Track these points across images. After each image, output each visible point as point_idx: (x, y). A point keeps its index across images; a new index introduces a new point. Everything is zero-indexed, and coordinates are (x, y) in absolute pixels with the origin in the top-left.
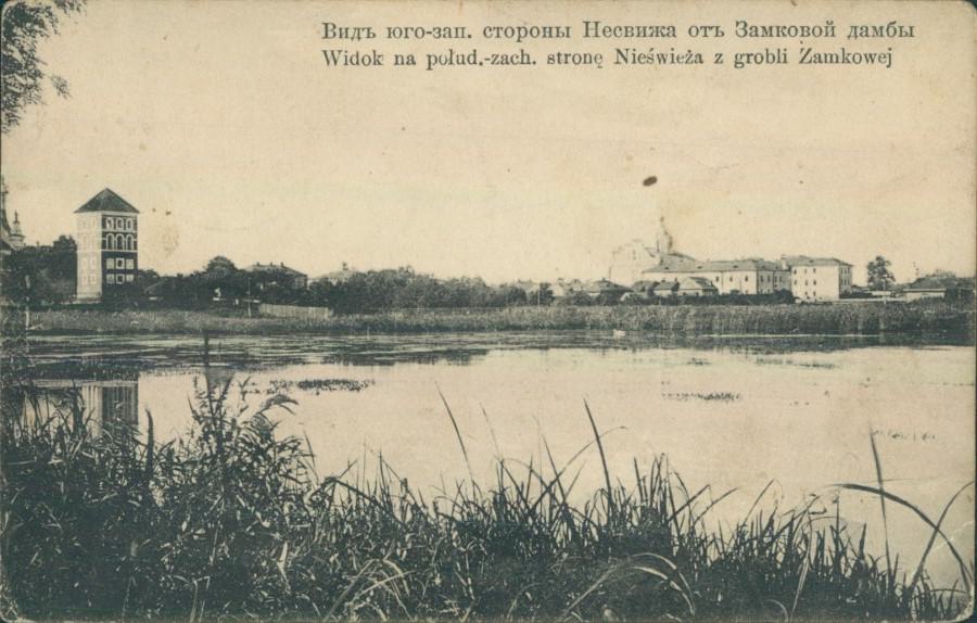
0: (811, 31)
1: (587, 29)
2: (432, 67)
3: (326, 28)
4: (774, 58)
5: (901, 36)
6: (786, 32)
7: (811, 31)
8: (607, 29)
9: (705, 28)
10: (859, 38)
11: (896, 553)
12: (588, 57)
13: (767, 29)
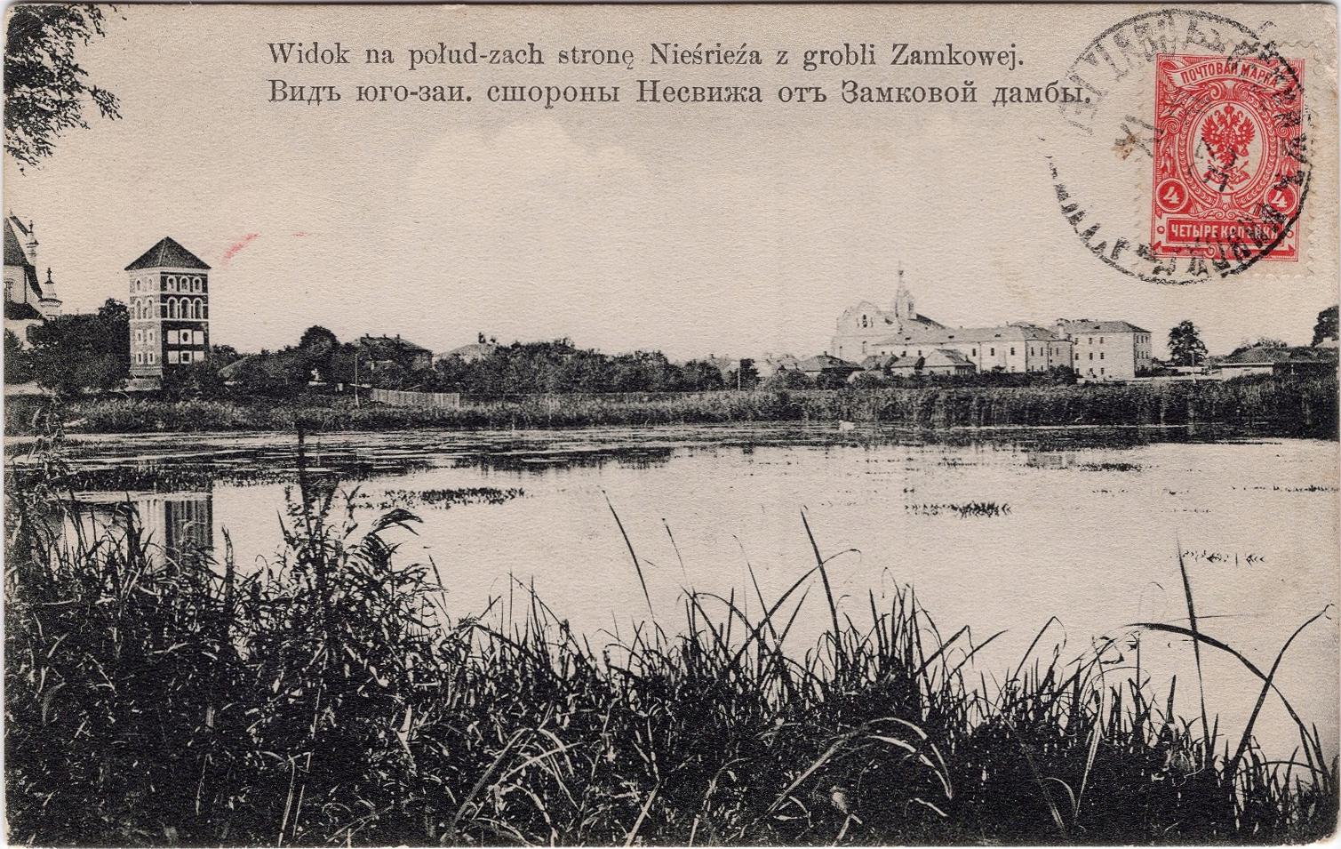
0: (943, 94)
7: (943, 94)
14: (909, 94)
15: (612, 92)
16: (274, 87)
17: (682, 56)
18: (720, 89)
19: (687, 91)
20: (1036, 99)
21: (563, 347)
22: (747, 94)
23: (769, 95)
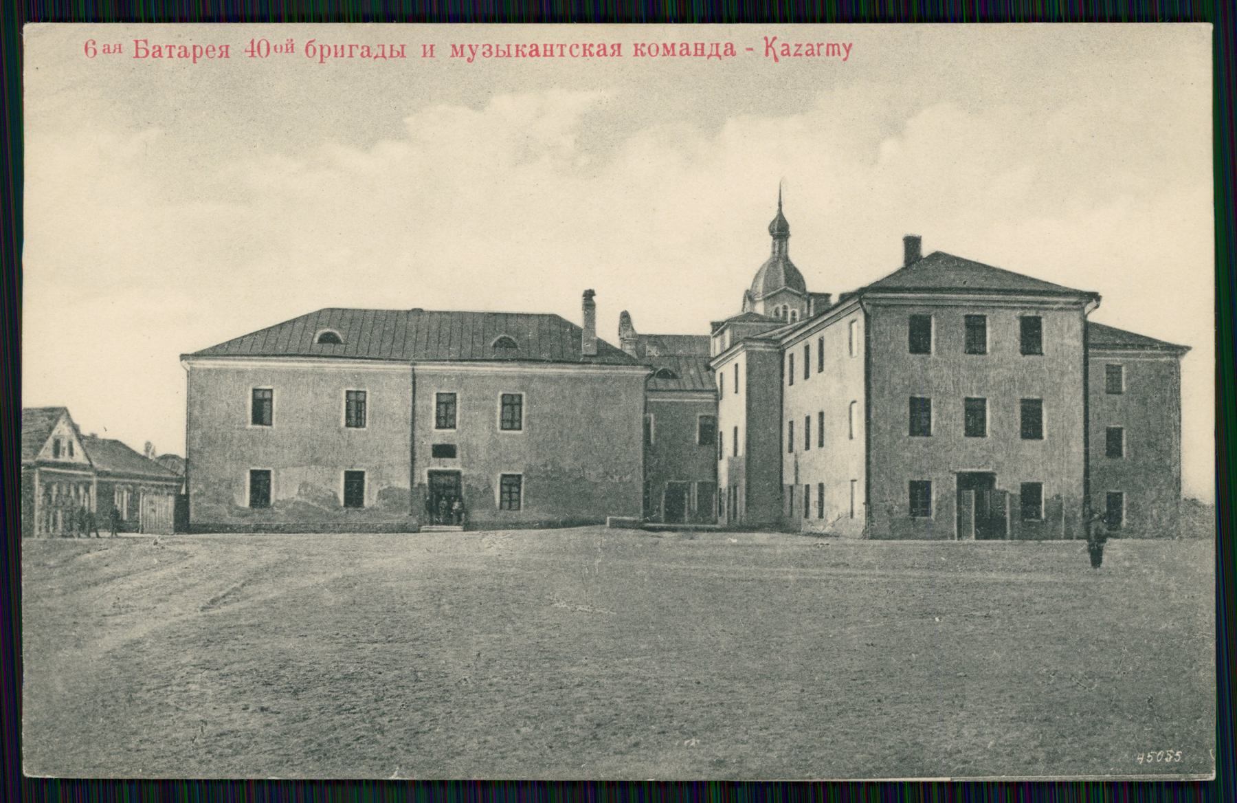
1: (137, 48)
2: (324, 60)
3: (432, 53)
4: (504, 52)
5: (497, 56)
6: (645, 50)
8: (210, 49)
9: (170, 46)
10: (723, 57)
11: (770, 56)
12: (198, 50)
13: (458, 48)
14: (645, 50)
15: (400, 49)
16: (137, 46)
17: (207, 51)
18: (552, 46)
19: (577, 46)
20: (671, 53)
21: (419, 311)
22: (527, 51)
23: (627, 50)
